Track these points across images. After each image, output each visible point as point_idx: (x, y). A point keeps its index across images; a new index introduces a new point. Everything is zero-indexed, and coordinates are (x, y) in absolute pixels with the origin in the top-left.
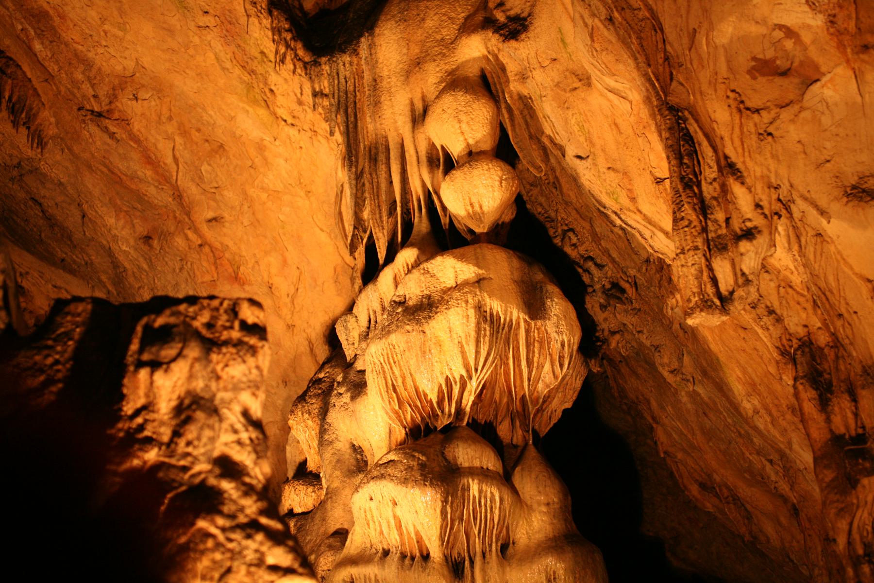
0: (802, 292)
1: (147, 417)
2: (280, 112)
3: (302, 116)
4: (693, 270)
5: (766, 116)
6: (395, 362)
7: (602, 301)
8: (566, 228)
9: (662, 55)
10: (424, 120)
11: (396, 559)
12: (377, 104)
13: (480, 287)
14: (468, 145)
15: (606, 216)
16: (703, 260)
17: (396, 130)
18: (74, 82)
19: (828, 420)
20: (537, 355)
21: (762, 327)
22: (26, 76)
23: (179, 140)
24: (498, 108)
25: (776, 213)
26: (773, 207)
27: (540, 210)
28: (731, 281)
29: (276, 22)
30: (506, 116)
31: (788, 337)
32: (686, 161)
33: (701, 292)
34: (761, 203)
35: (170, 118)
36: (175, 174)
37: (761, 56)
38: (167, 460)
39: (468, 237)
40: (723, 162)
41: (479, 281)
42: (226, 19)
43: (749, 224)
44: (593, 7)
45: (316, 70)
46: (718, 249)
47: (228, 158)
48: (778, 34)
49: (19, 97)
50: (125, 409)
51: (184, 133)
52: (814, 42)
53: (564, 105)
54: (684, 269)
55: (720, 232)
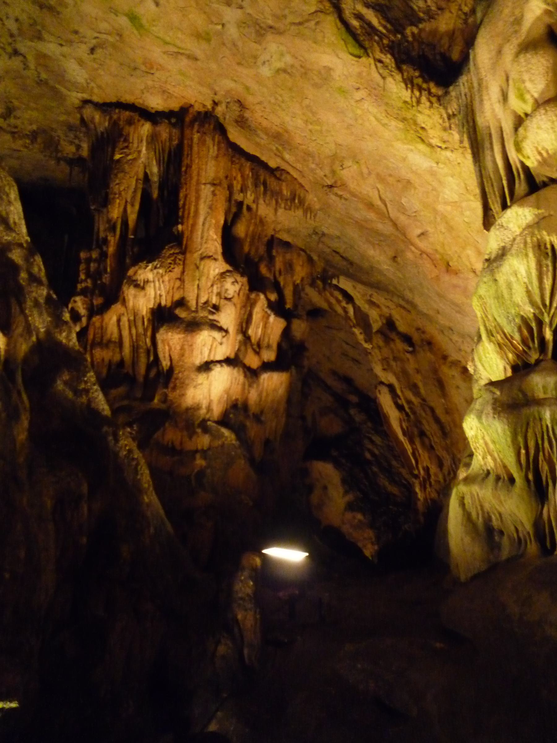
2: (435, 142)
12: (482, 101)
18: (312, 170)
22: (293, 177)
29: (405, 74)
35: (370, 173)
36: (385, 210)
42: (372, 88)
47: (415, 188)
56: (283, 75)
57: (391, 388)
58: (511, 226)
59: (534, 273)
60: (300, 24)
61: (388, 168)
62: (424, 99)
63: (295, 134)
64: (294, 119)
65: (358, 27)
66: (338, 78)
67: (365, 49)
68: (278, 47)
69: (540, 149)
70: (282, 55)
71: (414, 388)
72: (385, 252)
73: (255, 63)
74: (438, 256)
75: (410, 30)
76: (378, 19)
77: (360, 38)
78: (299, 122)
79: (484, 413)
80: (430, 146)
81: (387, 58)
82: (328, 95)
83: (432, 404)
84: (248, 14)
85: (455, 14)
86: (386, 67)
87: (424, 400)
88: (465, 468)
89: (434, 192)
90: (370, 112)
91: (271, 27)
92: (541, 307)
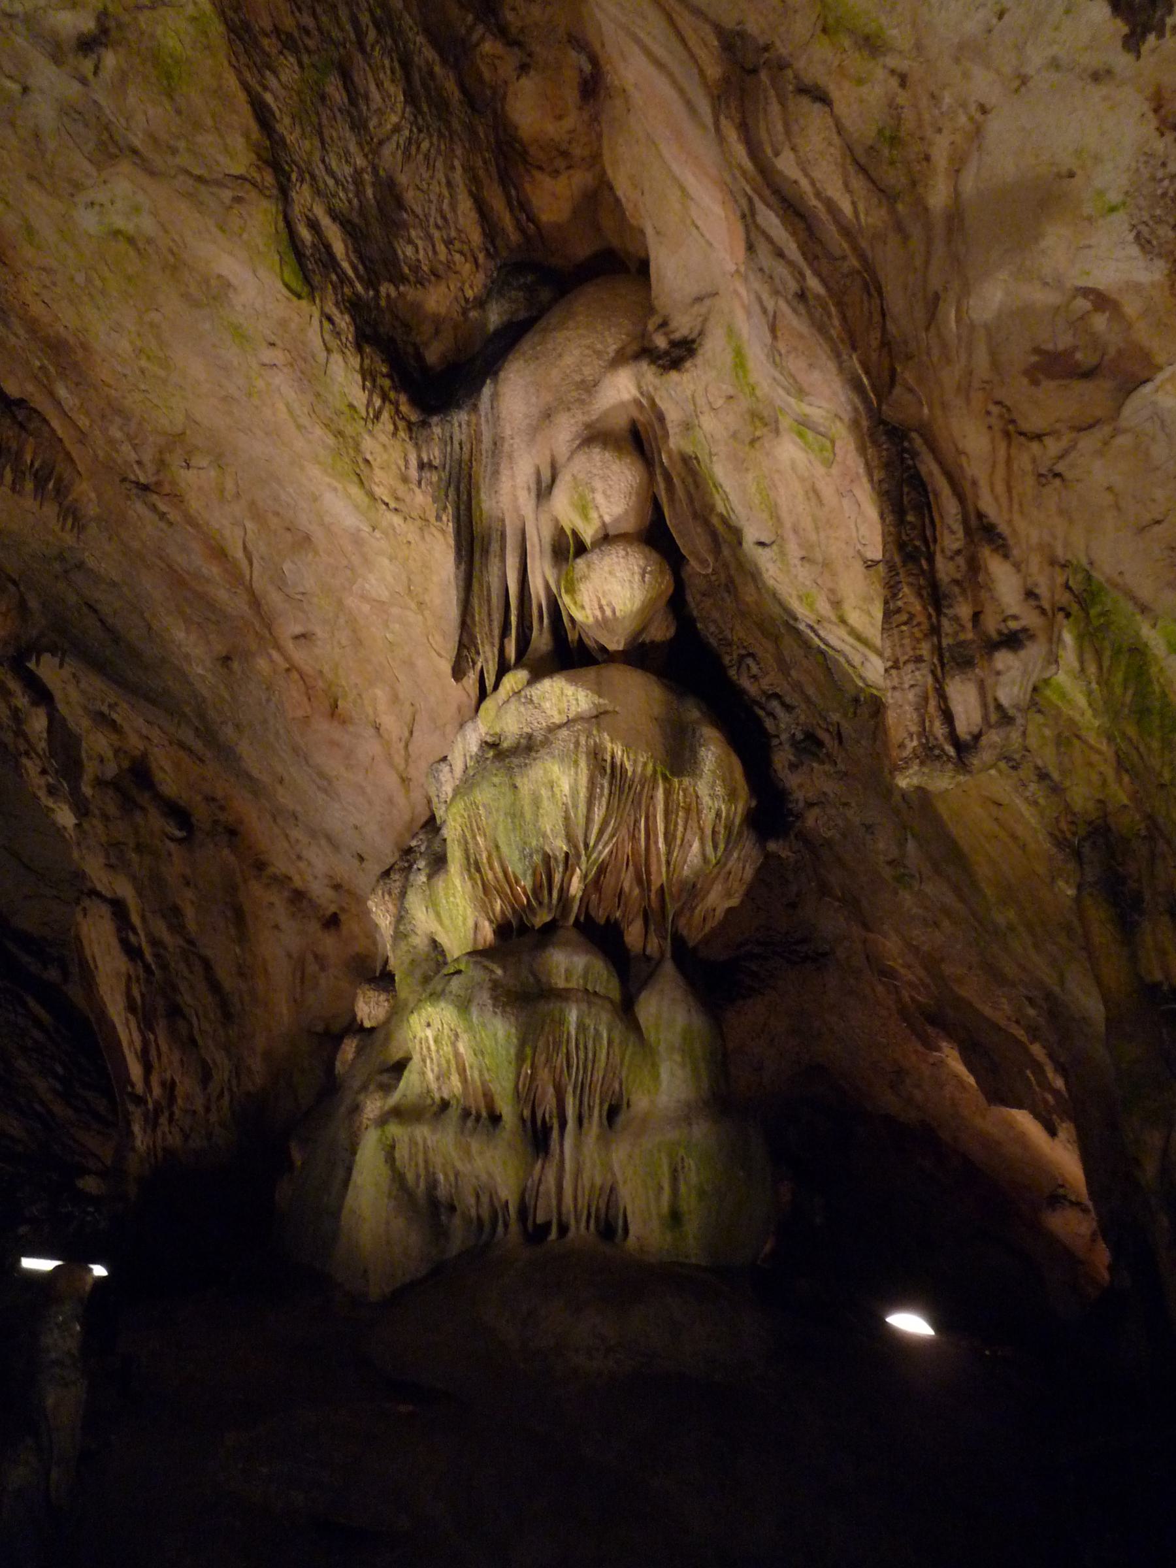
0: (1098, 746)
2: (379, 491)
3: (408, 499)
4: (911, 696)
5: (1053, 447)
6: (479, 829)
7: (792, 758)
8: (743, 652)
9: (879, 335)
10: (550, 493)
11: (455, 1119)
12: (496, 472)
13: (598, 724)
14: (604, 525)
15: (798, 632)
16: (930, 680)
17: (517, 509)
18: (111, 442)
19: (1133, 958)
20: (680, 828)
21: (1026, 798)
25: (1061, 609)
26: (1057, 597)
27: (712, 629)
28: (977, 716)
29: (367, 362)
30: (662, 485)
31: (1069, 818)
32: (910, 518)
33: (923, 733)
34: (1037, 591)
36: (247, 572)
37: (1050, 347)
40: (974, 522)
42: (299, 355)
43: (1013, 625)
44: (777, 281)
45: (425, 433)
46: (958, 664)
47: (316, 553)
48: (1083, 304)
49: (44, 462)
53: (740, 465)
54: (897, 694)
55: (962, 637)
56: (123, 246)
57: (118, 908)
58: (547, 705)
59: (583, 793)
60: (200, 179)
61: (276, 499)
62: (385, 416)
63: (103, 361)
64: (114, 335)
65: (308, 244)
66: (239, 308)
67: (313, 289)
68: (134, 193)
69: (604, 602)
70: (136, 209)
71: (172, 914)
72: (208, 642)
73: (72, 195)
74: (320, 684)
75: (386, 288)
76: (346, 246)
77: (308, 266)
78: (124, 346)
79: (475, 1003)
81: (343, 319)
82: (208, 326)
83: (209, 953)
84: (95, 102)
85: (453, 295)
86: (338, 334)
87: (191, 942)
88: (381, 1094)
89: (349, 572)
90: (283, 393)
91: (135, 152)
92: (582, 845)
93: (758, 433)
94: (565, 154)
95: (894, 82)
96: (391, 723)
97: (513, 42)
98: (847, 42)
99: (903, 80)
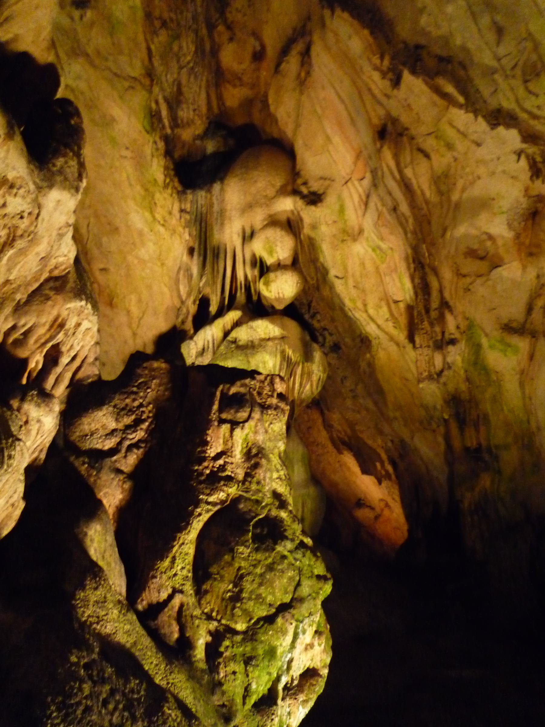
1: (227, 460)
5: (468, 280)
8: (316, 311)
12: (222, 224)
17: (232, 241)
23: (92, 220)
24: (296, 240)
38: (244, 494)
39: (270, 311)
41: (283, 338)
43: (453, 337)
50: (209, 451)
51: (97, 216)
52: (504, 245)
53: (335, 247)
58: (259, 330)
60: (115, 74)
70: (79, 77)
80: (154, 217)
89: (133, 247)
90: (127, 170)
91: (87, 55)
93: (345, 238)
94: (240, 79)
95: (452, 160)
96: (135, 311)
97: (229, 28)
98: (442, 143)
99: (456, 160)
